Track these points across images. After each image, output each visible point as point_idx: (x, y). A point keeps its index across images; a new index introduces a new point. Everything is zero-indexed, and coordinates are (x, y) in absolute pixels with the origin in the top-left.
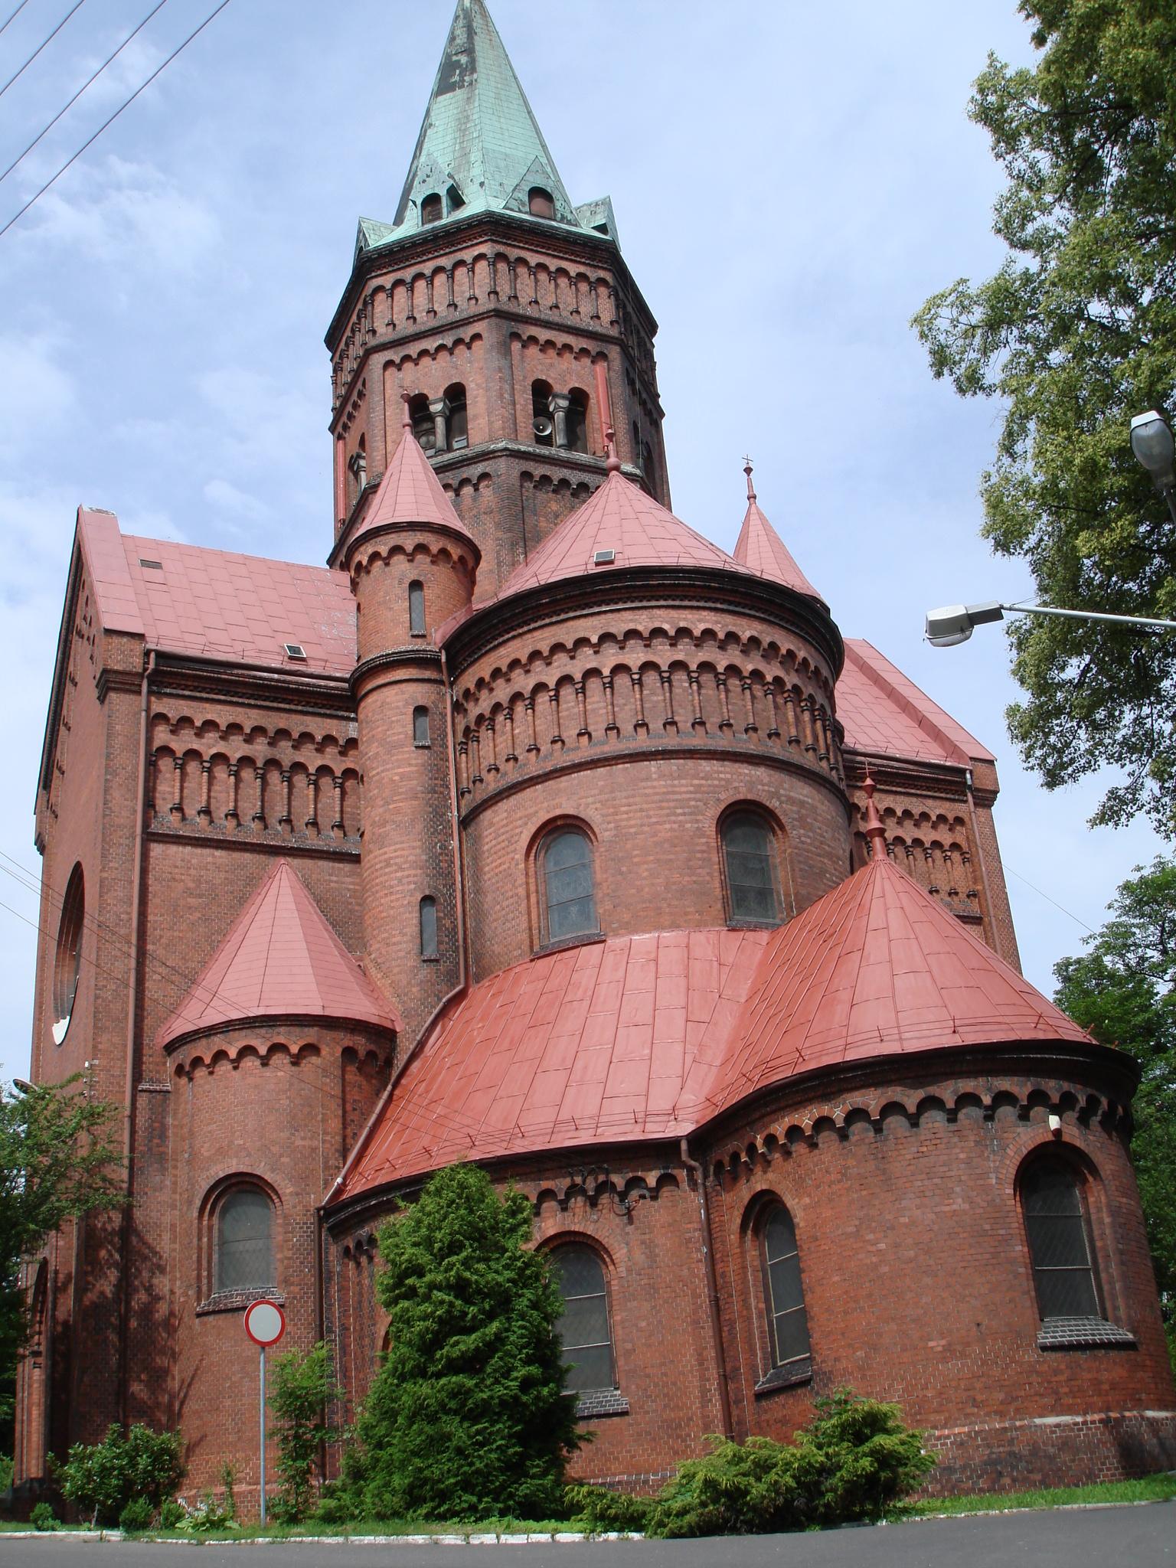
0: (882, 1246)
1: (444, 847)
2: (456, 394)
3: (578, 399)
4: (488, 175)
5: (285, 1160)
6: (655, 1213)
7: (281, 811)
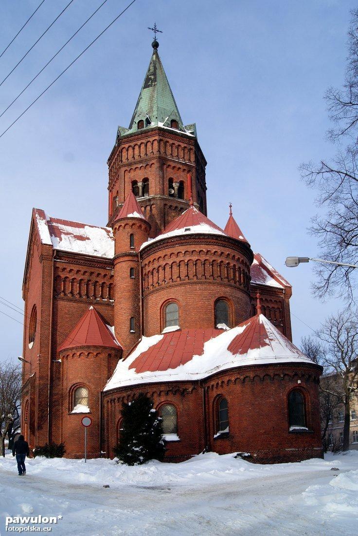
1: (138, 305)
2: (146, 180)
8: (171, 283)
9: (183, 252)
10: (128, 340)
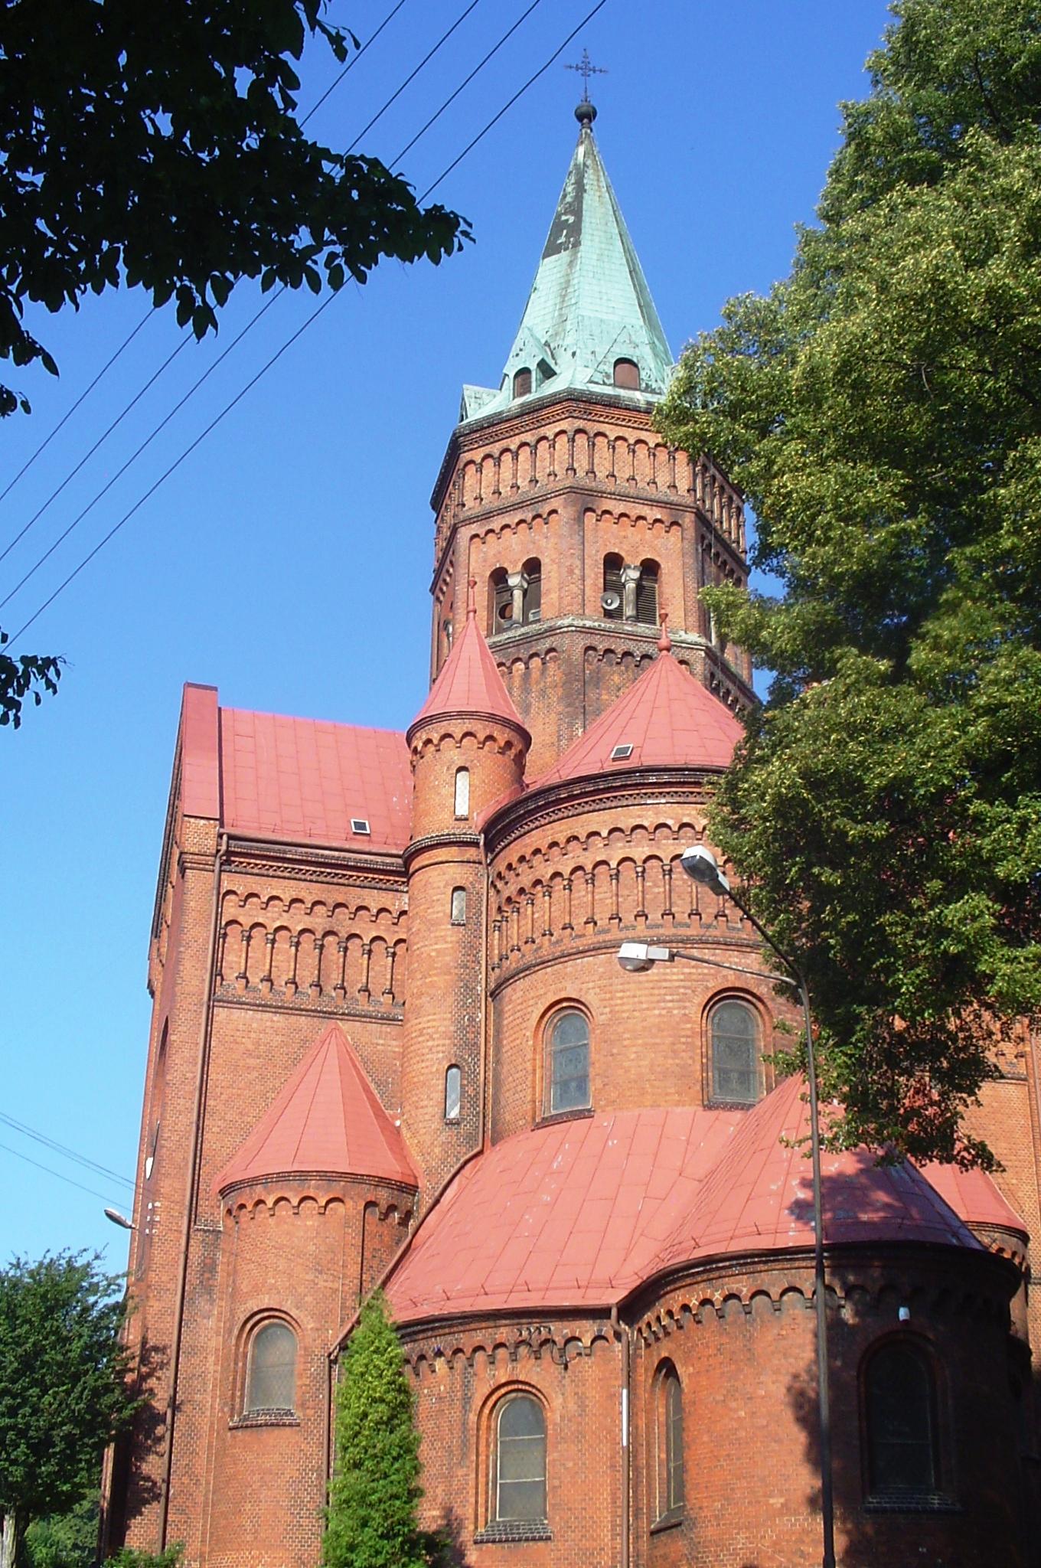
0: (743, 1414)
1: (472, 1019)
2: (533, 567)
3: (650, 568)
4: (580, 344)
5: (309, 1299)
6: (588, 1369)
7: (335, 978)
8: (615, 930)
9: (604, 834)
10: (437, 1150)
